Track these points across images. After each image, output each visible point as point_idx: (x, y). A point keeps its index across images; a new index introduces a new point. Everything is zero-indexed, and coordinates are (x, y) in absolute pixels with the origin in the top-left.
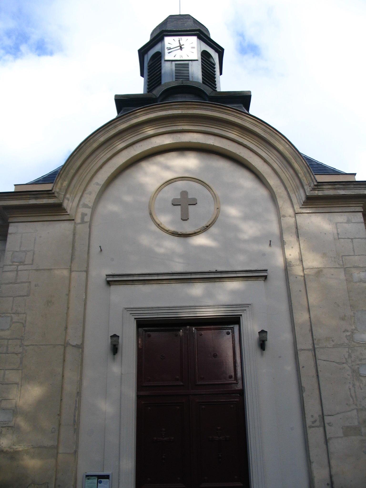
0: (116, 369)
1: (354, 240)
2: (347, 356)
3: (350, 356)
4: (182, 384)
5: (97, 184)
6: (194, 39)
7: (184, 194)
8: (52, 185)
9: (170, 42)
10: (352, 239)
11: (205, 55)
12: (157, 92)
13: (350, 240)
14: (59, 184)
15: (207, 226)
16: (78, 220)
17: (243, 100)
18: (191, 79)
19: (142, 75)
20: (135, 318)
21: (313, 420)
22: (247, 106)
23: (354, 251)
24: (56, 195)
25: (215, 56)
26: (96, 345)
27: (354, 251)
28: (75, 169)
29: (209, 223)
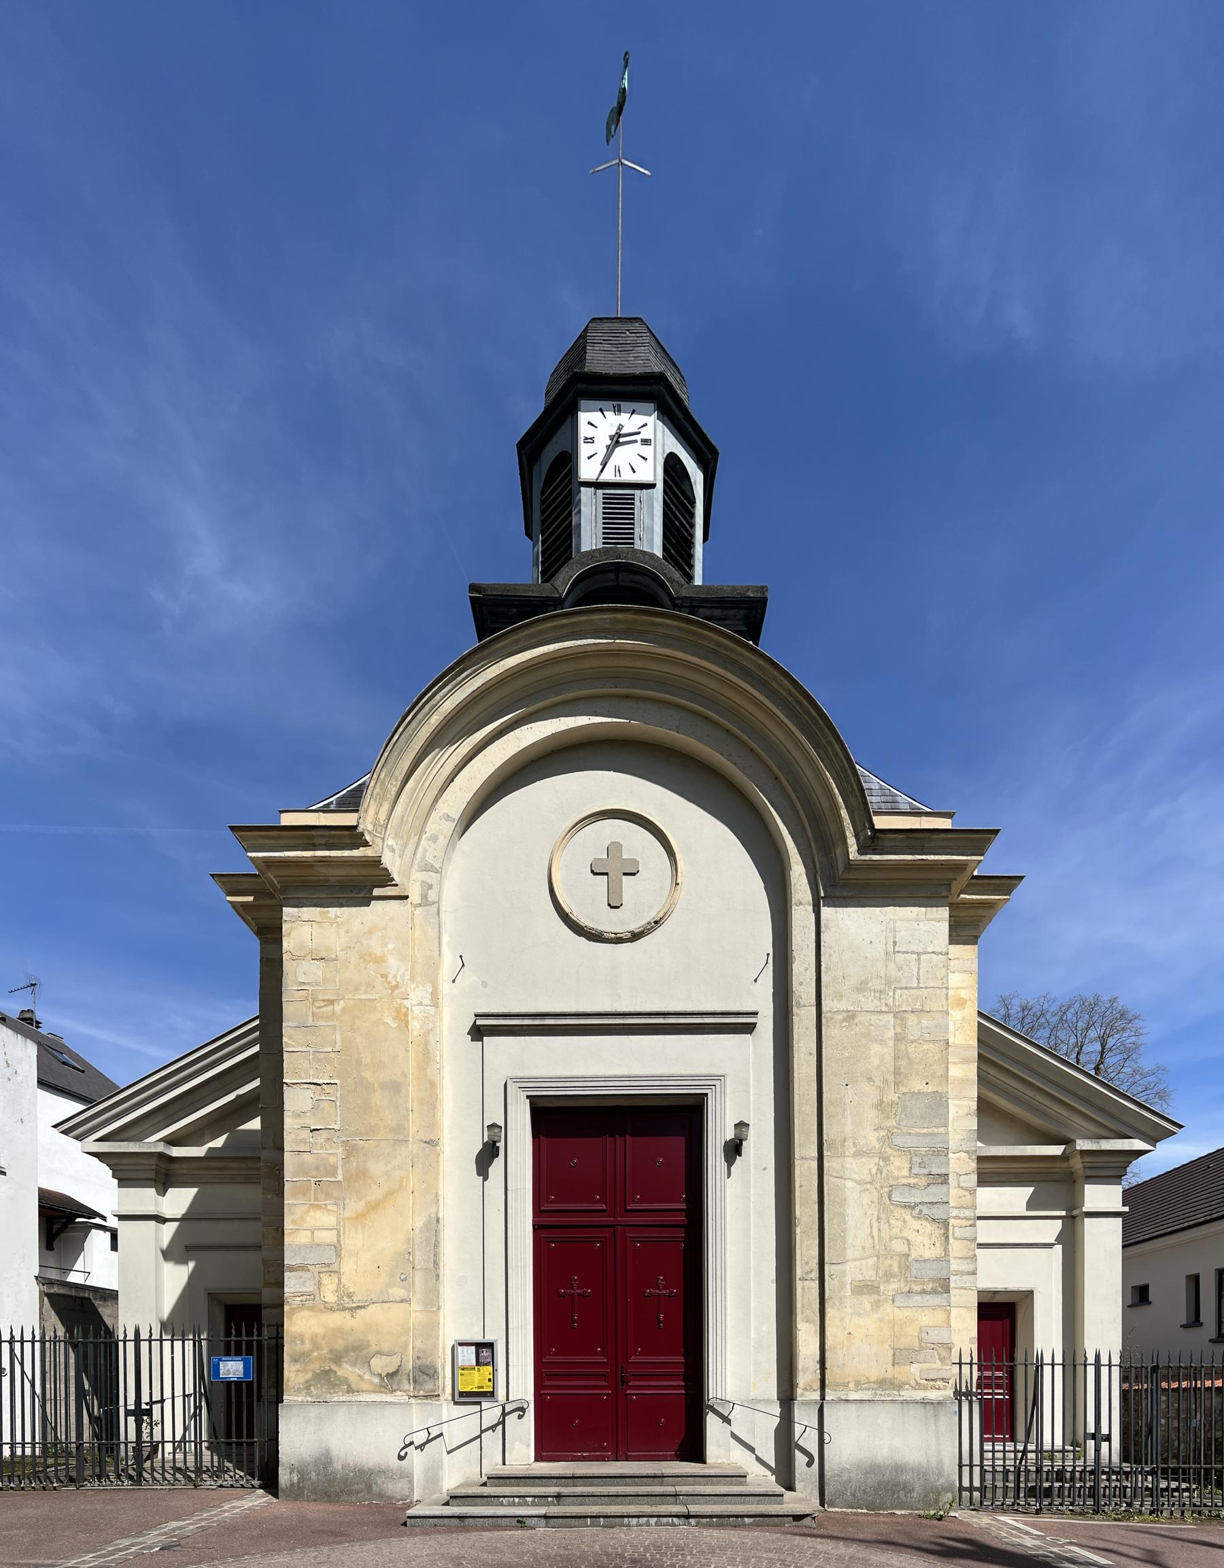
0: (1219, 1434)
1: (923, 957)
2: (874, 1171)
3: (880, 1171)
4: (604, 1207)
5: (448, 817)
6: (645, 422)
7: (613, 849)
8: (356, 815)
9: (595, 425)
10: (918, 954)
11: (672, 465)
12: (564, 581)
13: (915, 956)
14: (372, 810)
15: (656, 922)
16: (415, 897)
17: (745, 613)
18: (337, 1465)
19: (529, 534)
20: (528, 1097)
21: (807, 1268)
22: (753, 628)
23: (918, 979)
24: (368, 837)
25: (697, 476)
26: (459, 1142)
27: (918, 979)
28: (401, 777)
29: (661, 915)
